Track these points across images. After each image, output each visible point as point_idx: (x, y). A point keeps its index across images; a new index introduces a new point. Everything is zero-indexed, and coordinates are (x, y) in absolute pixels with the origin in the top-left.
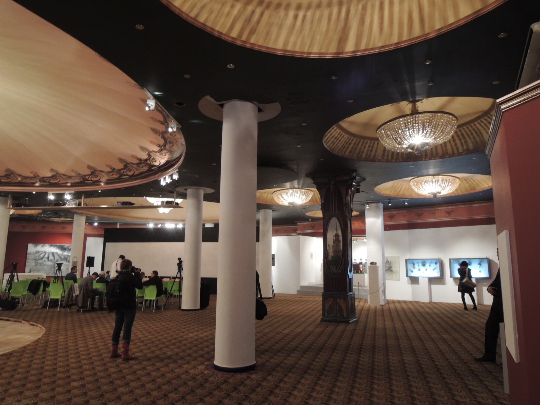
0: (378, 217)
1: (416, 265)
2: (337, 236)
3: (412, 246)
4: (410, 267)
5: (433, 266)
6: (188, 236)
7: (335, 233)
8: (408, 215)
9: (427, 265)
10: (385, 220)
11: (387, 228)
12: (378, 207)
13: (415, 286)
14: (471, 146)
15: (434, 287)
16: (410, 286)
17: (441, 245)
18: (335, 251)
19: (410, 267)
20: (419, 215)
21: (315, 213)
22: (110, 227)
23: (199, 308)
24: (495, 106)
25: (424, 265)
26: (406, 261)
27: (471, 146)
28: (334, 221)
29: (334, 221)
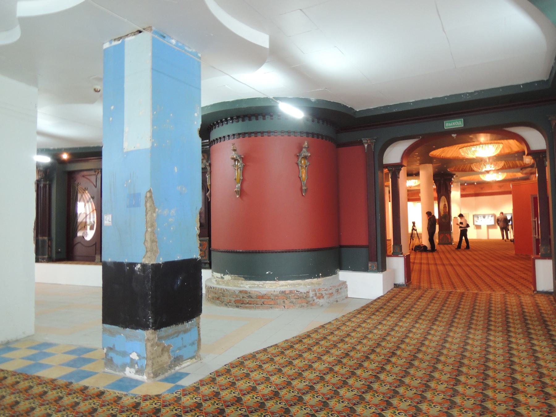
0: (457, 191)
1: (479, 218)
2: (445, 205)
3: (476, 207)
4: (476, 219)
5: (490, 218)
6: (422, 195)
7: (443, 204)
8: (477, 190)
9: (487, 217)
10: (461, 191)
11: (462, 196)
12: (457, 185)
13: (479, 230)
14: (511, 165)
15: (490, 230)
16: (476, 230)
17: (494, 206)
18: (444, 212)
19: (476, 219)
20: (482, 188)
21: (443, 152)
22: (290, 282)
23: (376, 263)
24: (222, 278)
25: (484, 217)
26: (474, 216)
27: (511, 165)
28: (443, 198)
29: (443, 198)
